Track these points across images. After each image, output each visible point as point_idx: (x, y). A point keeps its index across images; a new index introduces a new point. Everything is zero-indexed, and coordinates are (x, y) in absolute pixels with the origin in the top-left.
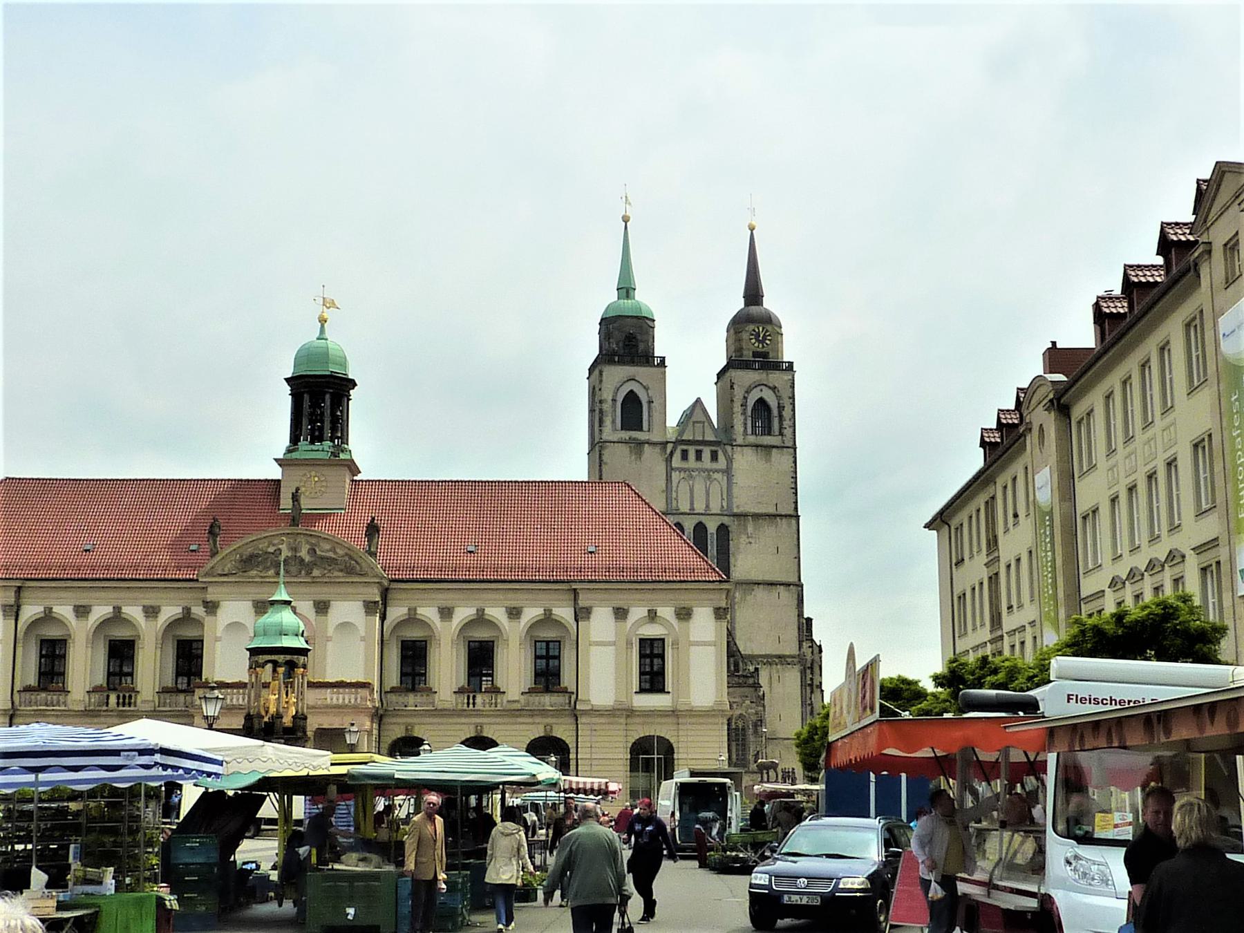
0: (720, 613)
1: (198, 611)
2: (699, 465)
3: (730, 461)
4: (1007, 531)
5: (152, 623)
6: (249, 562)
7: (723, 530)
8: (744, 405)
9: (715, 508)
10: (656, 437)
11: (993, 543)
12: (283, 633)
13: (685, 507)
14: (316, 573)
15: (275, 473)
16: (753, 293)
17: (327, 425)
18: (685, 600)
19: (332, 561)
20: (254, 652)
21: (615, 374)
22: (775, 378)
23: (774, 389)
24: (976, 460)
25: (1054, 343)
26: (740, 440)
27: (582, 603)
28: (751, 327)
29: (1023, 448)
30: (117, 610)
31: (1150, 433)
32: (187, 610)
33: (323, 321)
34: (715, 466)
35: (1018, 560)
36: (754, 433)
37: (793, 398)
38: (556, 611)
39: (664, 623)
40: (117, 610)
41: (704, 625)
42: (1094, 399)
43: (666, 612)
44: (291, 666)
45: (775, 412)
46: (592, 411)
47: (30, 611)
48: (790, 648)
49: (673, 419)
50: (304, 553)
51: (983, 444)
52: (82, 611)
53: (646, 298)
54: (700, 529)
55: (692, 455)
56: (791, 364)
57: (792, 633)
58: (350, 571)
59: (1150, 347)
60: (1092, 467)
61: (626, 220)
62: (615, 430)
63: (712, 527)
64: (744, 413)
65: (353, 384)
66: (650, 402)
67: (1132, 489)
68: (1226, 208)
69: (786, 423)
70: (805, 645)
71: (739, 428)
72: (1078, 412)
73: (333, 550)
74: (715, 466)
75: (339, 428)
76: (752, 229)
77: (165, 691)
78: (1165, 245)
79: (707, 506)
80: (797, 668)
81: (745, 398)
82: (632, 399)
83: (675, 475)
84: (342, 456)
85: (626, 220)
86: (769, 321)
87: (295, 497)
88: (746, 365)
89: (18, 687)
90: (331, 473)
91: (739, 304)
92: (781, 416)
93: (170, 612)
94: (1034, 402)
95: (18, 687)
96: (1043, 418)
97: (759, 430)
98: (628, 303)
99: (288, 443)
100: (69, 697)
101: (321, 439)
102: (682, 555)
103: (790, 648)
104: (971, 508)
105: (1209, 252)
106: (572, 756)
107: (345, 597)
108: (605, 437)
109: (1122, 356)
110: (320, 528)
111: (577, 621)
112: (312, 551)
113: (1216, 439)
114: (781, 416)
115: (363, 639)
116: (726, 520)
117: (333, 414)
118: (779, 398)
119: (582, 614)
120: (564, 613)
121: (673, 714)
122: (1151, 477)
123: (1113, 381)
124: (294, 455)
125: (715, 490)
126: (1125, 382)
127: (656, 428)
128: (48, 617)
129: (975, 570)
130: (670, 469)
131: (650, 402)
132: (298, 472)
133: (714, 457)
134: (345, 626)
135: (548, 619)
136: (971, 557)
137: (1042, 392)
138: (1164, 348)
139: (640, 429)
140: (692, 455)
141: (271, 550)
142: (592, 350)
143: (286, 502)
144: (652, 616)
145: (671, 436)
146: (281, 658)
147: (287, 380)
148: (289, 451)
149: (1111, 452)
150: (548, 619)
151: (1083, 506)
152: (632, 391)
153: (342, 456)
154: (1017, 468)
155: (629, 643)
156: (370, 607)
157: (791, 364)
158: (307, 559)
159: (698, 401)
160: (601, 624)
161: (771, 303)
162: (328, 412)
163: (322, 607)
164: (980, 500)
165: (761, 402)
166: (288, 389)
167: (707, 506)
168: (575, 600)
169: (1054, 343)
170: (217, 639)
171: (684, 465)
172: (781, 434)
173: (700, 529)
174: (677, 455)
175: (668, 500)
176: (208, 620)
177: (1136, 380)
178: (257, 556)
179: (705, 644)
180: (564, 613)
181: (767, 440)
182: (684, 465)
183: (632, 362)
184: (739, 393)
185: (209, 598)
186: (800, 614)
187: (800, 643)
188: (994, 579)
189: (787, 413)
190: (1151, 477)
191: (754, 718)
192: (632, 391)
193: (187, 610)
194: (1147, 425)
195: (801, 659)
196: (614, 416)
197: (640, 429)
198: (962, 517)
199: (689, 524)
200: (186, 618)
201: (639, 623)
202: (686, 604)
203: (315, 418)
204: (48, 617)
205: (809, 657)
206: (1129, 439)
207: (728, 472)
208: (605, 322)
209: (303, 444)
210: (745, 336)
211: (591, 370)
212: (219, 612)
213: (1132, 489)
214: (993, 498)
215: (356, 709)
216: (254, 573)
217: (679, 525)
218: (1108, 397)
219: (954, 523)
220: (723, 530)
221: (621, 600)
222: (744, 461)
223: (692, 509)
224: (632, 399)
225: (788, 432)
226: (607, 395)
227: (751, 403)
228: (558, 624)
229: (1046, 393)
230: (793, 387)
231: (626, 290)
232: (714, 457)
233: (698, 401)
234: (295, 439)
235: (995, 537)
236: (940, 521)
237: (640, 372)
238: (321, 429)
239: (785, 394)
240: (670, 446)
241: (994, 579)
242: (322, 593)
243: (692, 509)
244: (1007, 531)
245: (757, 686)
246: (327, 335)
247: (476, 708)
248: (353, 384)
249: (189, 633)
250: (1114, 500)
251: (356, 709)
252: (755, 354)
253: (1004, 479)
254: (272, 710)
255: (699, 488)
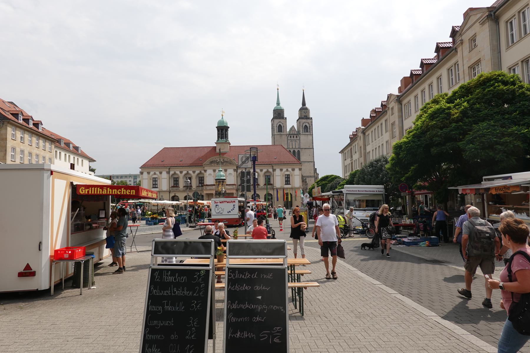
0: (300, 169)
1: (203, 172)
2: (293, 139)
3: (300, 138)
4: (354, 154)
5: (194, 174)
6: (212, 162)
7: (299, 151)
8: (302, 126)
9: (297, 147)
10: (285, 133)
11: (352, 157)
12: (221, 176)
13: (291, 147)
14: (224, 164)
15: (215, 145)
16: (304, 104)
17: (224, 136)
18: (294, 167)
19: (227, 162)
20: (216, 180)
21: (277, 121)
22: (309, 121)
23: (308, 123)
24: (349, 141)
25: (363, 118)
26: (302, 134)
27: (274, 168)
28: (303, 111)
29: (357, 140)
30: (188, 172)
31: (379, 139)
32: (201, 172)
33: (222, 115)
34: (297, 139)
35: (356, 160)
36: (304, 132)
37: (312, 125)
38: (269, 170)
39: (290, 171)
40: (188, 172)
41: (297, 171)
42: (369, 132)
43: (290, 169)
44: (223, 182)
45: (309, 128)
46: (272, 128)
47: (172, 173)
48: (313, 175)
49: (288, 130)
50: (222, 160)
51: (350, 138)
52: (181, 172)
53: (282, 105)
54: (294, 151)
55: (292, 137)
56: (312, 118)
57: (313, 171)
58: (230, 164)
59: (379, 124)
60: (369, 144)
61: (278, 89)
62: (277, 132)
63: (296, 151)
64: (302, 128)
65: (229, 127)
66: (284, 126)
67: (376, 149)
68: (391, 102)
69: (311, 130)
70: (315, 173)
71: (301, 131)
72: (367, 134)
73: (227, 160)
74: (297, 139)
75: (226, 137)
76: (303, 90)
77: (197, 187)
78: (382, 105)
79: (295, 147)
80: (314, 178)
81: (303, 125)
82: (280, 126)
83: (289, 141)
84: (228, 142)
85: (278, 89)
86: (307, 109)
87: (220, 150)
88: (302, 118)
89: (170, 187)
90: (225, 145)
91: (301, 106)
92: (310, 128)
93: (197, 172)
94: (359, 131)
95: (170, 187)
96: (360, 134)
97: (305, 131)
98: (279, 106)
99: (217, 139)
100: (180, 188)
101: (223, 138)
102: (292, 159)
103: (313, 175)
104: (348, 150)
105: (389, 109)
106: (273, 197)
107: (230, 168)
108: (275, 133)
109: (375, 124)
110: (225, 156)
111: (273, 171)
112: (223, 160)
113: (390, 142)
114: (310, 128)
115: (234, 176)
116: (299, 149)
117: (225, 133)
118: (309, 125)
119: (274, 170)
120: (271, 170)
121: (292, 188)
122: (379, 147)
123: (373, 129)
124: (219, 142)
125: (297, 144)
126: (375, 129)
127: (285, 132)
128: (175, 173)
129: (348, 161)
130: (288, 140)
131: (284, 126)
132: (219, 145)
133: (297, 137)
134: (230, 174)
135: (268, 171)
136: (348, 159)
137: (360, 130)
138: (381, 124)
139: (282, 132)
140: (292, 137)
141: (216, 160)
142: (272, 117)
143: (218, 151)
144: (287, 170)
145: (288, 133)
146: (221, 181)
147: (216, 127)
148: (217, 141)
149: (372, 142)
150: (268, 171)
151: (367, 151)
152: (280, 125)
153: (228, 142)
154: (356, 143)
155: (283, 175)
156: (234, 170)
157: (312, 118)
158: (222, 161)
159: (293, 126)
160: (278, 172)
161: (307, 105)
162: (224, 133)
163: (226, 171)
164: (349, 148)
165: (306, 126)
166: (216, 129)
167: (295, 147)
168: (273, 167)
169: (363, 118)
170: (207, 177)
171: (291, 139)
172: (310, 132)
173: (294, 151)
174: (289, 137)
175: (288, 146)
176: (205, 173)
177: (377, 129)
178: (213, 161)
179: (297, 175)
180: (271, 170)
181: (307, 133)
182: (291, 139)
183: (280, 119)
184: (301, 124)
185: (205, 169)
186: (314, 167)
187: (314, 173)
188: (352, 163)
189: (311, 128)
190: (379, 147)
191: (306, 188)
192: (280, 125)
193: (201, 172)
194: (379, 137)
195: (314, 176)
196: (276, 129)
197: (282, 132)
198: (346, 151)
199: (292, 151)
200: (201, 173)
201: (285, 172)
202: (294, 168)
203: (222, 135)
204: (175, 173)
205: (316, 176)
206: (375, 140)
207: (299, 140)
208: (274, 110)
209: (220, 140)
210: (302, 113)
211: (272, 120)
212: (207, 172)
213: (376, 149)
214: (352, 148)
215: (233, 189)
216: (213, 164)
217: (290, 151)
218: (372, 132)
219: (344, 152)
220: (299, 151)
221: (281, 167)
222: (302, 137)
223: (292, 147)
224: (280, 126)
225: (311, 132)
226: (275, 125)
227: (304, 126)
228: (270, 172)
229: (361, 130)
230: (312, 122)
231: (278, 104)
232: (297, 137)
233: (293, 126)
234: (218, 139)
235: (352, 155)
236: (342, 152)
237: (281, 120)
238: (223, 136)
239: (311, 124)
240: (288, 135)
241: (352, 163)
242: (225, 168)
243: (292, 147)
244: (354, 154)
245: (306, 182)
246: (223, 118)
247: (236, 184)
248: (229, 127)
249: (201, 176)
250: (373, 150)
251: (233, 189)
252: (304, 116)
253: (354, 145)
254: (220, 190)
255: (294, 143)
